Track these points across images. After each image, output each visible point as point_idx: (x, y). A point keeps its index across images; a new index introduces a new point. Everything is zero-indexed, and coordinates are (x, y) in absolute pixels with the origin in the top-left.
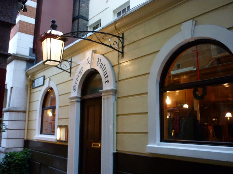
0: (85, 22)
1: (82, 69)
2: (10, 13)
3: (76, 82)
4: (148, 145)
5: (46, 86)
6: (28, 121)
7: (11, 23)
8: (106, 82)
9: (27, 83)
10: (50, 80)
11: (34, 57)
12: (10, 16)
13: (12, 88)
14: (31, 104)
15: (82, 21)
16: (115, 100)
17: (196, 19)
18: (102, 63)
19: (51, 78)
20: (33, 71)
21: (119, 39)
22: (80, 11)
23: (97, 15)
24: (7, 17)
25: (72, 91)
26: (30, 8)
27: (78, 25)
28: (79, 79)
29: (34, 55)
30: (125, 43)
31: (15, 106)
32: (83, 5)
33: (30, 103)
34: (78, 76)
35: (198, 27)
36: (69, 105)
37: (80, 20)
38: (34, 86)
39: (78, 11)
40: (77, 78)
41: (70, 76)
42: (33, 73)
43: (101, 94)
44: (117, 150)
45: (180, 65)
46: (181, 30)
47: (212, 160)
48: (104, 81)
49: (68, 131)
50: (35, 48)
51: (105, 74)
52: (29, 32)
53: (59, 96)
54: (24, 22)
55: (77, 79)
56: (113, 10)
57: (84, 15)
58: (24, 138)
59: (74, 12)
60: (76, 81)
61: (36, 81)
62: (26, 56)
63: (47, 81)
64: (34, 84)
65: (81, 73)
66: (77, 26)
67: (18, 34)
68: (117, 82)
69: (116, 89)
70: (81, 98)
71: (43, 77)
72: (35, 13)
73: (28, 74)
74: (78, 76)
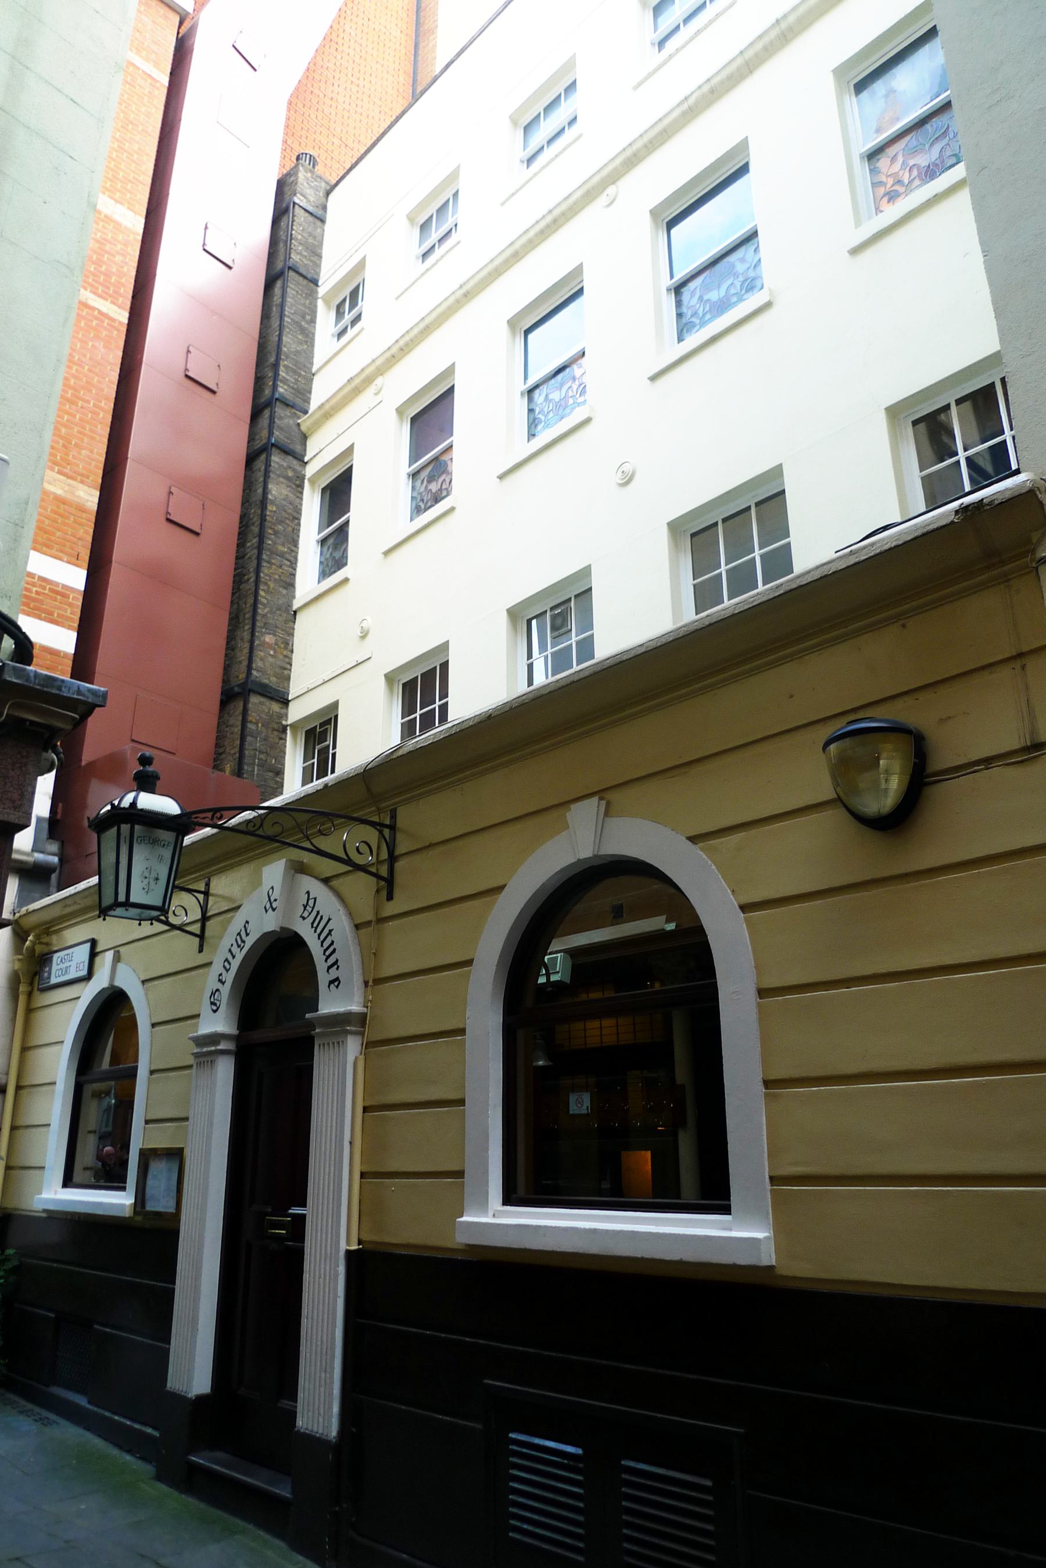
0: (276, 707)
1: (245, 927)
2: (15, 791)
3: (221, 975)
5: (100, 981)
7: (16, 821)
8: (331, 982)
9: (17, 967)
10: (117, 959)
11: (54, 854)
12: (14, 802)
14: (31, 1054)
15: (261, 703)
16: (361, 1054)
17: (609, 796)
18: (318, 912)
20: (46, 916)
21: (381, 832)
22: (254, 666)
23: (325, 683)
24: (4, 804)
25: (206, 1009)
26: (49, 656)
27: (244, 722)
28: (235, 964)
29: (54, 847)
32: (269, 639)
33: (25, 1049)
34: (230, 951)
35: (615, 824)
36: (190, 1067)
37: (254, 699)
38: (49, 978)
39: (245, 663)
40: (227, 960)
41: (201, 951)
44: (360, 1242)
45: (621, 907)
47: (681, 1263)
48: (323, 978)
49: (445, 71)
50: (59, 816)
51: (327, 953)
53: (153, 1025)
56: (386, 672)
57: (272, 681)
59: (227, 668)
65: (243, 942)
66: (239, 723)
68: (370, 983)
70: (237, 1039)
71: (88, 945)
74: (230, 951)
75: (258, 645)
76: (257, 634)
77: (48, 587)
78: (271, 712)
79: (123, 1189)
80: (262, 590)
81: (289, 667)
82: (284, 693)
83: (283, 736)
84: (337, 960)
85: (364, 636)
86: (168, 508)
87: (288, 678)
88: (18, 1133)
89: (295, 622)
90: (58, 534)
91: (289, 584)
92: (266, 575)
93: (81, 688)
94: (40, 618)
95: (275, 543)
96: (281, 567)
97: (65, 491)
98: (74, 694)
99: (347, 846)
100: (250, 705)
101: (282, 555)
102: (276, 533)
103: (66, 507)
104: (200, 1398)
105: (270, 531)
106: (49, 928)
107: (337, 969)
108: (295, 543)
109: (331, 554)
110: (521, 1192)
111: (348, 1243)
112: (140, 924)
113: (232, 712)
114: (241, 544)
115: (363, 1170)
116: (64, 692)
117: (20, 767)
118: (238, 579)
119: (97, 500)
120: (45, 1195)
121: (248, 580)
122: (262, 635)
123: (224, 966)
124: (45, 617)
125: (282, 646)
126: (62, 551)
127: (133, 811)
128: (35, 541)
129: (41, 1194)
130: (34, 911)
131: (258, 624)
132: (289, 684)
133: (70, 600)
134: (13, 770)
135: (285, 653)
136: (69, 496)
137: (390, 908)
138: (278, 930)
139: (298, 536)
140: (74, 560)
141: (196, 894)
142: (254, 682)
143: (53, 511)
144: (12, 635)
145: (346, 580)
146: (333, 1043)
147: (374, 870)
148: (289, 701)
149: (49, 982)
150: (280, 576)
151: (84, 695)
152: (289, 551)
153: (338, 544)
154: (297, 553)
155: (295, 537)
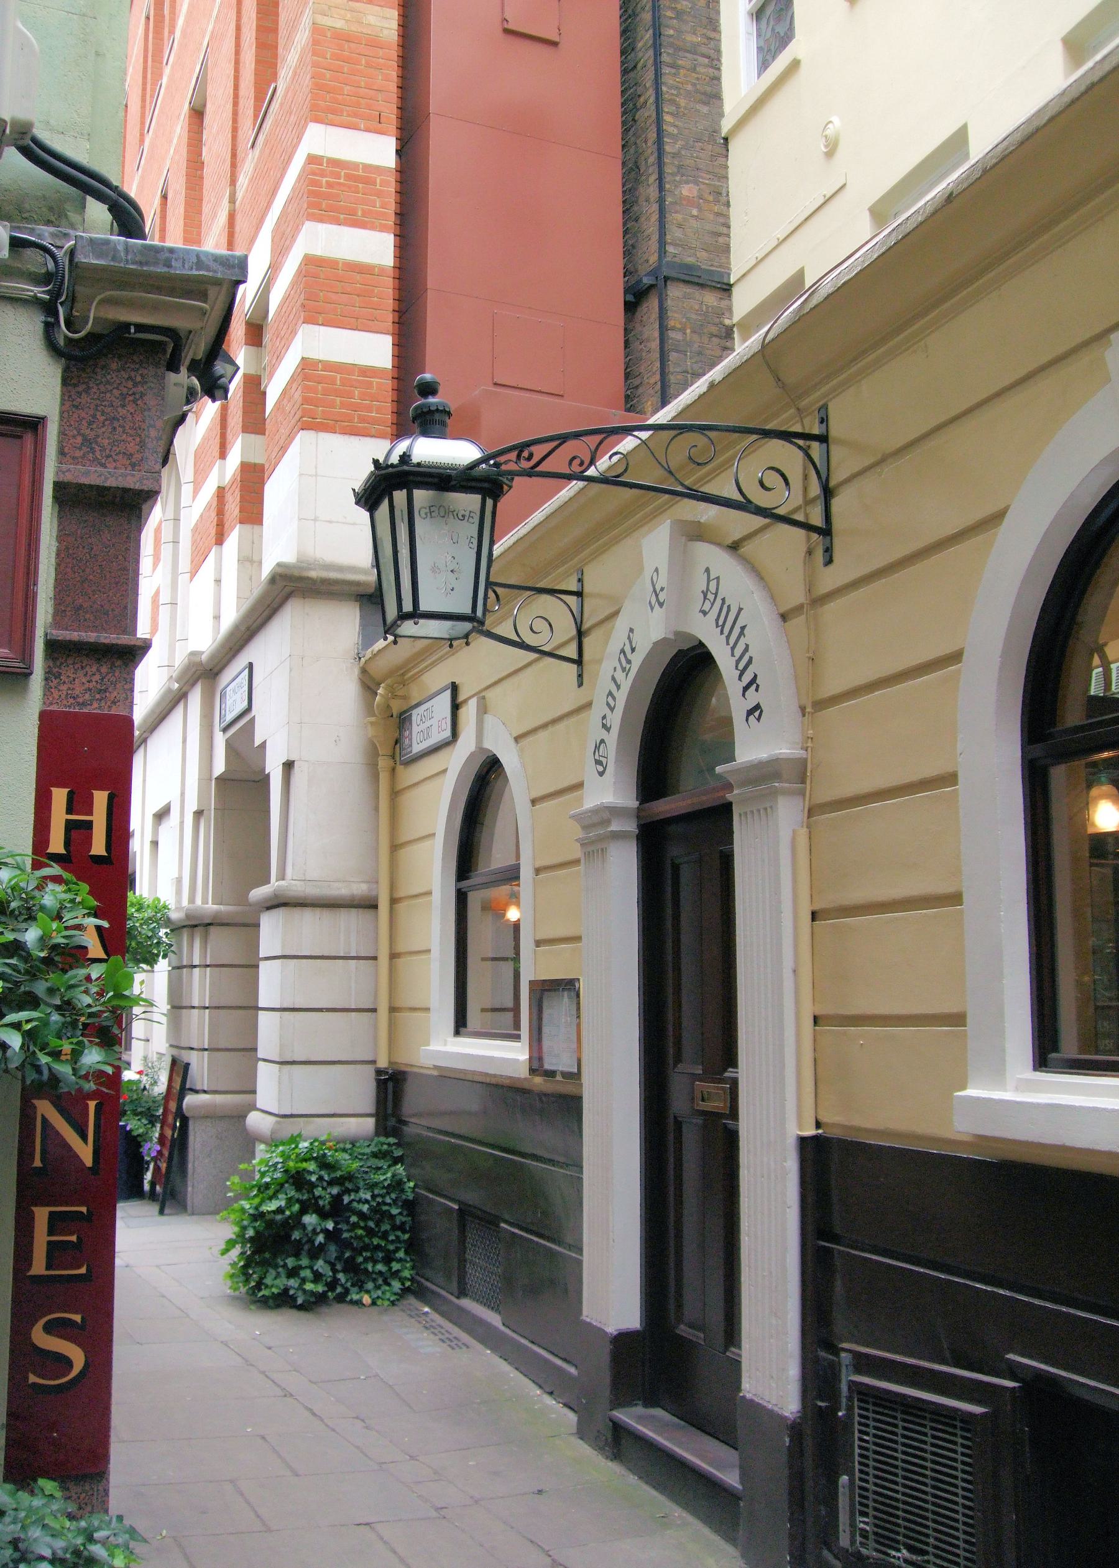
0: (710, 299)
1: (629, 638)
3: (604, 717)
4: (964, 1088)
6: (393, 956)
7: (137, 486)
8: (750, 713)
10: (483, 710)
13: (289, 766)
14: (402, 853)
15: (687, 296)
19: (489, 694)
21: (806, 452)
22: (668, 238)
25: (591, 769)
26: (358, 277)
27: (663, 329)
28: (622, 696)
30: (843, 465)
31: (313, 874)
32: (687, 190)
33: (395, 847)
34: (613, 679)
36: (577, 862)
38: (411, 746)
39: (655, 237)
40: (610, 694)
42: (399, 668)
43: (729, 787)
44: (818, 1125)
46: (1108, 380)
48: (738, 707)
51: (741, 666)
52: (362, 420)
53: (534, 802)
54: (329, 366)
55: (610, 700)
58: (374, 1062)
59: (629, 252)
60: (607, 711)
61: (416, 715)
62: (353, 569)
63: (469, 712)
64: (407, 733)
65: (629, 662)
66: (657, 334)
67: (304, 441)
68: (809, 710)
69: (798, 753)
70: (639, 813)
71: (448, 694)
72: (390, 303)
73: (372, 679)
74: (613, 679)
75: (671, 203)
76: (667, 186)
77: (343, 174)
78: (704, 308)
79: (517, 1038)
80: (668, 113)
81: (724, 230)
82: (721, 275)
83: (728, 344)
84: (756, 676)
85: (831, 152)
86: (503, 13)
87: (727, 249)
88: (400, 962)
89: (727, 156)
90: (347, 89)
91: (713, 97)
92: (671, 87)
93: (203, 258)
94: (338, 223)
95: (679, 31)
96: (694, 70)
97: (347, 21)
98: (192, 269)
99: (740, 480)
100: (669, 302)
101: (693, 50)
102: (679, 15)
103: (352, 45)
104: (579, 1422)
105: (669, 14)
106: (403, 675)
107: (757, 690)
108: (713, 24)
109: (773, 30)
110: (1069, 1045)
111: (800, 1127)
112: (451, 646)
113: (645, 319)
114: (627, 50)
115: (817, 1013)
116: (176, 269)
117: (135, 401)
118: (630, 106)
119: (394, 25)
120: (435, 1046)
121: (646, 102)
122: (676, 186)
123: (608, 704)
124: (345, 218)
125: (711, 198)
126: (356, 115)
127: (406, 468)
128: (314, 108)
129: (428, 1045)
130: (379, 651)
131: (668, 169)
132: (728, 258)
133: (378, 187)
134: (123, 406)
135: (716, 209)
136: (354, 28)
137: (830, 578)
138: (672, 636)
139: (718, 13)
140: (375, 124)
141: (563, 597)
142: (672, 265)
143: (336, 57)
144: (100, 197)
145: (795, 65)
146: (759, 811)
147: (799, 517)
148: (731, 286)
149: (411, 752)
150: (694, 85)
151: (208, 269)
152: (706, 41)
153: (781, 10)
154: (719, 41)
155: (713, 16)
